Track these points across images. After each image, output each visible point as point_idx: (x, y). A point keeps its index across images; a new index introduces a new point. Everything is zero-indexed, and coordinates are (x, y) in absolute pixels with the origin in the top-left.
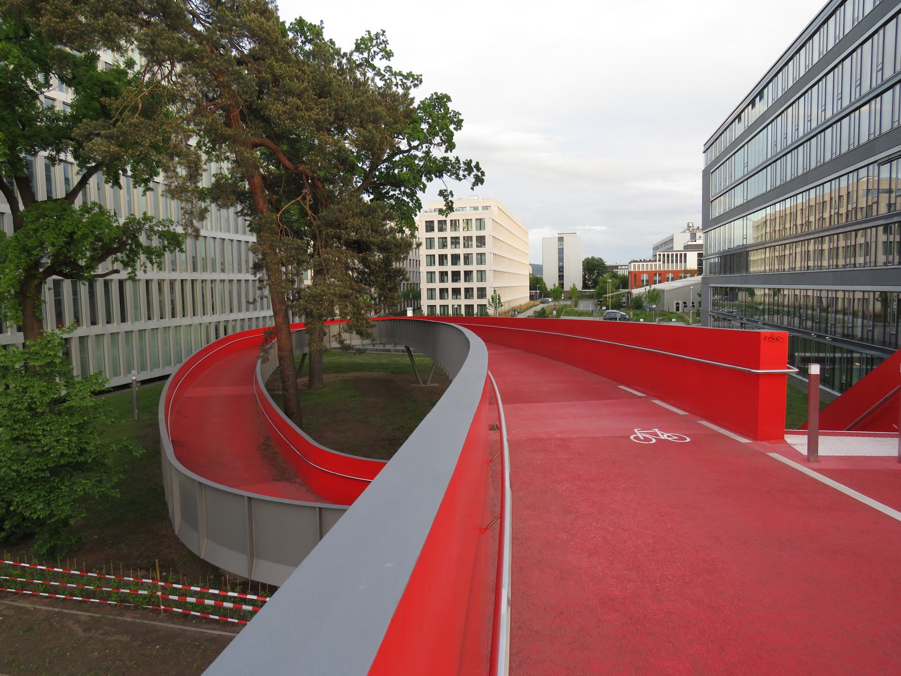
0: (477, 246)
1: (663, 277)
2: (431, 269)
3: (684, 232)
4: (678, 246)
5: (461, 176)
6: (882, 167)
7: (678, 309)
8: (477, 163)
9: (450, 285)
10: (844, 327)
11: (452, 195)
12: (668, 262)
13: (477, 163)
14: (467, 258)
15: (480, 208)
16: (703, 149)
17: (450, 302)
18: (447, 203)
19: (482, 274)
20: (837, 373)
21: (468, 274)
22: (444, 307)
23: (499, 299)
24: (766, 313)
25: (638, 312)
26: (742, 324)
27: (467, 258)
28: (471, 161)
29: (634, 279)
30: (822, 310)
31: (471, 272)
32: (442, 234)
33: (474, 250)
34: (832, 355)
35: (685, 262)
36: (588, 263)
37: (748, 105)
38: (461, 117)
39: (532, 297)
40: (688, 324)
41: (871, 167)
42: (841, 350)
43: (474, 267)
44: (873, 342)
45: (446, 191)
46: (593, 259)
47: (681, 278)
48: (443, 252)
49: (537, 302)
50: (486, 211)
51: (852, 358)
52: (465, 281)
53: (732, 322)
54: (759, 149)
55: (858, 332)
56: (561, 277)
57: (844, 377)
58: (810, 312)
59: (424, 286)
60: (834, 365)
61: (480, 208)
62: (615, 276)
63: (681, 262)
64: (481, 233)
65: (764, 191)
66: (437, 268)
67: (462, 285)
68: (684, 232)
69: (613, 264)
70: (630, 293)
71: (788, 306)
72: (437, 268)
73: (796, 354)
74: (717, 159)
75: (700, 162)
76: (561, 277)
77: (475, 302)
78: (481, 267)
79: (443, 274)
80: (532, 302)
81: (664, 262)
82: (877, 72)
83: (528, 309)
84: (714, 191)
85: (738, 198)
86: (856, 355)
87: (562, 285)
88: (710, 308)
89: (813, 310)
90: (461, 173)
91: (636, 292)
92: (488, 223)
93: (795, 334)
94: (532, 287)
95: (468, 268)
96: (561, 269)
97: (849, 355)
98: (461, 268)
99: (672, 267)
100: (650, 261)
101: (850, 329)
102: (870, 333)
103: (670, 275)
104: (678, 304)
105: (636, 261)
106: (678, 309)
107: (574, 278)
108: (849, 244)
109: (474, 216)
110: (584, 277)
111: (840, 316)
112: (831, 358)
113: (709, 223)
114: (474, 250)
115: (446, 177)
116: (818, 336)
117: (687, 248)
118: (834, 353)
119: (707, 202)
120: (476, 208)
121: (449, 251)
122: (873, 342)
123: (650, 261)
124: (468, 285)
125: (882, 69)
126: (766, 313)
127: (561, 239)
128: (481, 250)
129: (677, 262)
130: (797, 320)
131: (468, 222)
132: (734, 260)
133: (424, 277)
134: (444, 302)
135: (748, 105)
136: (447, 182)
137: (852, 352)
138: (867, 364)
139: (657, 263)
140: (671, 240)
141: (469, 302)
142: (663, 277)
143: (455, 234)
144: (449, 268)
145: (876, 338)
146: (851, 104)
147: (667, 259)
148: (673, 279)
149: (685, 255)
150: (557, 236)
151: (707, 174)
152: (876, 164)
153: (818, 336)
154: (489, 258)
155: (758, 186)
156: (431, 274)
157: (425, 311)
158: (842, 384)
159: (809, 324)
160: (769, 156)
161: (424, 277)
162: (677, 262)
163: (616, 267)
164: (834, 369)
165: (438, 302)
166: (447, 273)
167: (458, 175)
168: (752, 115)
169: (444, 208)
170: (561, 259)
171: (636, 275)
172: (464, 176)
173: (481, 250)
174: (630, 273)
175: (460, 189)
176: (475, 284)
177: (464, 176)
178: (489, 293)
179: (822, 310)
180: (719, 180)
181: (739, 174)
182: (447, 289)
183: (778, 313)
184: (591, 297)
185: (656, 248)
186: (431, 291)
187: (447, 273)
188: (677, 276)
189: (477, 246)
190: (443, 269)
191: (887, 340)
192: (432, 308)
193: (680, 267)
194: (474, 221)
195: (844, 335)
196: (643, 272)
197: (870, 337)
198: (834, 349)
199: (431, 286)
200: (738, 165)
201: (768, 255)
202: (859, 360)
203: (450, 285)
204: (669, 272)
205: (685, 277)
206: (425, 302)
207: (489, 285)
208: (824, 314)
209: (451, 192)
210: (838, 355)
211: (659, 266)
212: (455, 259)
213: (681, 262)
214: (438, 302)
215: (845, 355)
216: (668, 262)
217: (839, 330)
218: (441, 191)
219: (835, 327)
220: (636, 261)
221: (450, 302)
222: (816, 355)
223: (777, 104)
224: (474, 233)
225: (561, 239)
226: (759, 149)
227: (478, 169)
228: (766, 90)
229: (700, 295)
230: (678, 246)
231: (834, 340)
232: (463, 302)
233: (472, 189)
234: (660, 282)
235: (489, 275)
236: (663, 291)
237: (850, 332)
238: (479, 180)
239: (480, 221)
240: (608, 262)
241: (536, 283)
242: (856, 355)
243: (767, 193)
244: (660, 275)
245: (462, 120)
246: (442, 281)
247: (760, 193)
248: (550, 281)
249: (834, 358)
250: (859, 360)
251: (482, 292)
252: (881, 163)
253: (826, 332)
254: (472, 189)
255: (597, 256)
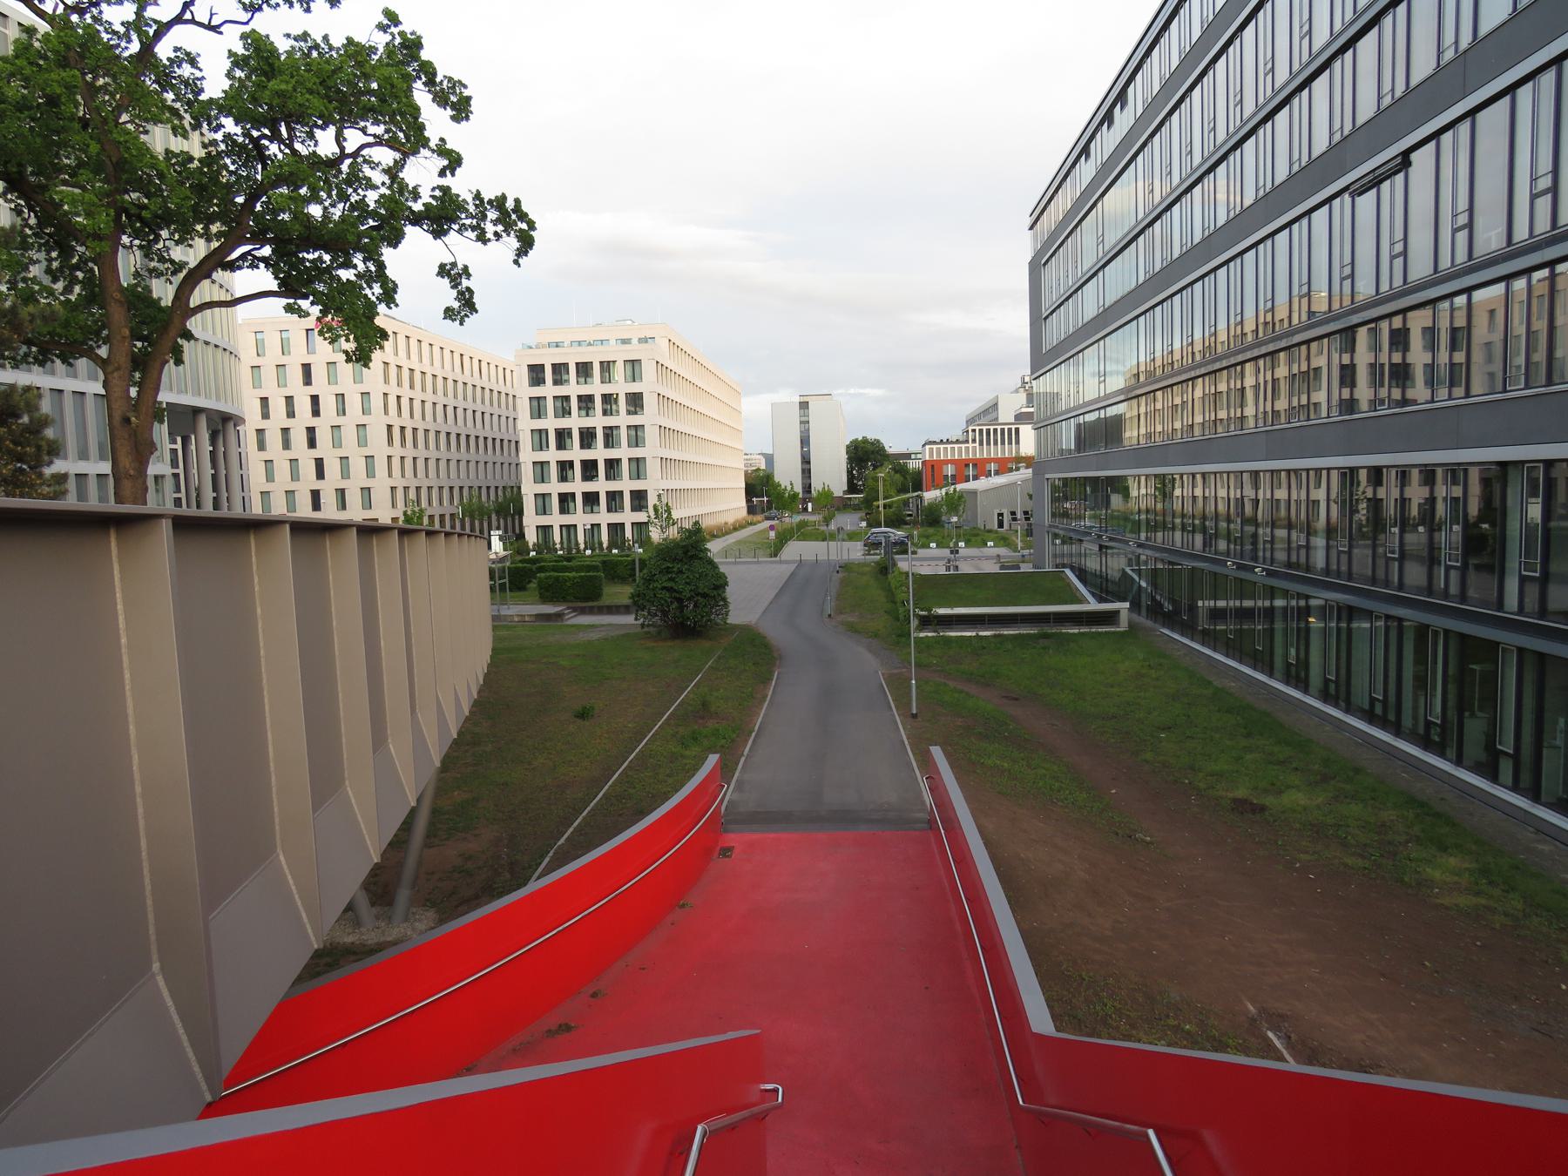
0: (629, 413)
1: (980, 468)
2: (542, 456)
3: (1017, 391)
4: (1006, 415)
5: (489, 235)
6: (1358, 199)
7: (1001, 525)
8: (517, 201)
9: (578, 486)
10: (1289, 549)
11: (469, 276)
12: (988, 443)
13: (517, 201)
14: (610, 436)
15: (635, 341)
16: (1029, 221)
17: (581, 519)
18: (461, 293)
19: (638, 465)
20: (1278, 639)
21: (612, 465)
22: (616, 529)
23: (668, 511)
24: (1143, 528)
25: (931, 530)
26: (1101, 547)
27: (610, 436)
28: (504, 197)
29: (933, 473)
30: (1245, 521)
31: (618, 461)
32: (561, 391)
33: (622, 420)
34: (1267, 603)
35: (1018, 442)
36: (856, 448)
37: (1101, 124)
38: (466, 93)
39: (751, 510)
40: (1016, 550)
41: (1336, 202)
42: (1286, 594)
43: (623, 452)
44: (1350, 577)
45: (454, 265)
46: (865, 440)
47: (1011, 470)
48: (564, 423)
49: (759, 517)
50: (644, 346)
51: (1308, 607)
52: (608, 478)
53: (1085, 545)
54: (1125, 202)
55: (1319, 560)
56: (806, 473)
57: (1293, 652)
58: (1223, 525)
59: (529, 489)
60: (1272, 622)
61: (635, 341)
62: (901, 470)
63: (1010, 443)
64: (634, 388)
65: (1134, 285)
66: (552, 455)
67: (601, 486)
68: (1017, 391)
69: (902, 450)
70: (921, 498)
71: (1183, 516)
72: (552, 455)
73: (1200, 603)
74: (1053, 236)
75: (1024, 248)
76: (806, 473)
77: (628, 517)
78: (637, 453)
79: (565, 467)
80: (750, 518)
81: (981, 443)
82: (1302, 39)
83: (735, 529)
84: (1049, 299)
85: (1089, 304)
86: (1313, 602)
87: (807, 488)
88: (1047, 520)
89: (1229, 520)
90: (490, 229)
91: (931, 495)
92: (648, 370)
93: (1195, 564)
94: (751, 491)
95: (613, 454)
96: (806, 461)
97: (1302, 603)
98: (599, 453)
99: (1003, 451)
100: (958, 442)
101: (1303, 552)
102: (1344, 558)
103: (993, 467)
104: (1001, 515)
105: (934, 443)
106: (1001, 525)
107: (832, 474)
108: (1295, 370)
109: (619, 355)
110: (850, 473)
111: (1281, 533)
112: (1265, 609)
113: (1043, 358)
114: (622, 420)
115: (452, 237)
116: (1240, 567)
117: (1021, 418)
118: (1272, 598)
119: (1038, 320)
120: (625, 342)
121: (575, 422)
122: (1350, 577)
123: (958, 442)
124: (614, 486)
125: (1310, 31)
126: (1143, 528)
127: (804, 405)
128: (635, 420)
129: (1003, 443)
130: (1199, 538)
131: (606, 366)
132: (1102, 434)
133: (527, 473)
134: (567, 519)
135: (1101, 124)
136: (459, 246)
137: (1307, 597)
138: (1339, 619)
139: (971, 445)
140: (995, 406)
141: (616, 518)
142: (980, 468)
143: (585, 390)
144: (576, 454)
145: (1355, 569)
146: (1204, 161)
147: (987, 438)
148: (997, 473)
149: (1017, 430)
150: (797, 399)
151: (1037, 267)
152: (1346, 196)
153: (1240, 567)
154: (651, 435)
155: (1123, 277)
156: (540, 437)
157: (531, 537)
158: (1289, 665)
159: (1222, 545)
160: (1141, 216)
161: (527, 473)
162: (1003, 443)
163: (908, 456)
164: (1272, 630)
165: (556, 520)
166: (571, 463)
167: (483, 232)
168: (1108, 141)
169: (456, 305)
170: (805, 441)
171: (934, 466)
172: (496, 234)
173: (635, 420)
174: (924, 463)
175: (487, 260)
176: (626, 485)
177: (496, 234)
178: (652, 500)
179: (1245, 521)
180: (1058, 277)
181: (1089, 262)
182: (597, 493)
183: (1164, 528)
184: (856, 508)
185: (970, 421)
186: (543, 499)
187: (571, 463)
188: (1004, 466)
189: (629, 413)
190: (564, 456)
191: (1381, 574)
192: (545, 530)
193: (1007, 451)
194: (620, 366)
195: (1289, 565)
196: (947, 462)
197: (1344, 568)
198: (1272, 593)
199: (542, 488)
200: (1087, 245)
201: (1143, 410)
202: (1323, 612)
203: (578, 486)
204: (989, 460)
205: (1018, 469)
206: (531, 521)
207: (653, 484)
208: (1250, 529)
209: (466, 268)
210: (1279, 603)
211: (973, 451)
212: (587, 437)
213: (1010, 443)
214: (556, 520)
215: (1294, 603)
216: (988, 443)
217: (1281, 556)
218: (442, 266)
219: (1272, 549)
220: (934, 443)
221: (581, 519)
222: (1238, 603)
223: (1151, 108)
224: (621, 386)
225: (804, 405)
226: (1125, 202)
227: (523, 216)
228: (1131, 90)
229: (1031, 497)
230: (1006, 415)
231: (1270, 573)
232: (604, 517)
233: (516, 262)
234: (976, 478)
235: (652, 468)
236: (974, 493)
237: (1303, 560)
238: (526, 243)
239: (634, 365)
240: (893, 446)
241: (760, 489)
242: (1313, 602)
243: (1138, 287)
244: (975, 465)
245: (469, 99)
246: (563, 478)
247: (1127, 290)
248: (788, 476)
249: (1272, 608)
250: (1323, 612)
251: (639, 498)
252: (1357, 190)
253: (1255, 559)
254: (516, 262)
255: (871, 436)
